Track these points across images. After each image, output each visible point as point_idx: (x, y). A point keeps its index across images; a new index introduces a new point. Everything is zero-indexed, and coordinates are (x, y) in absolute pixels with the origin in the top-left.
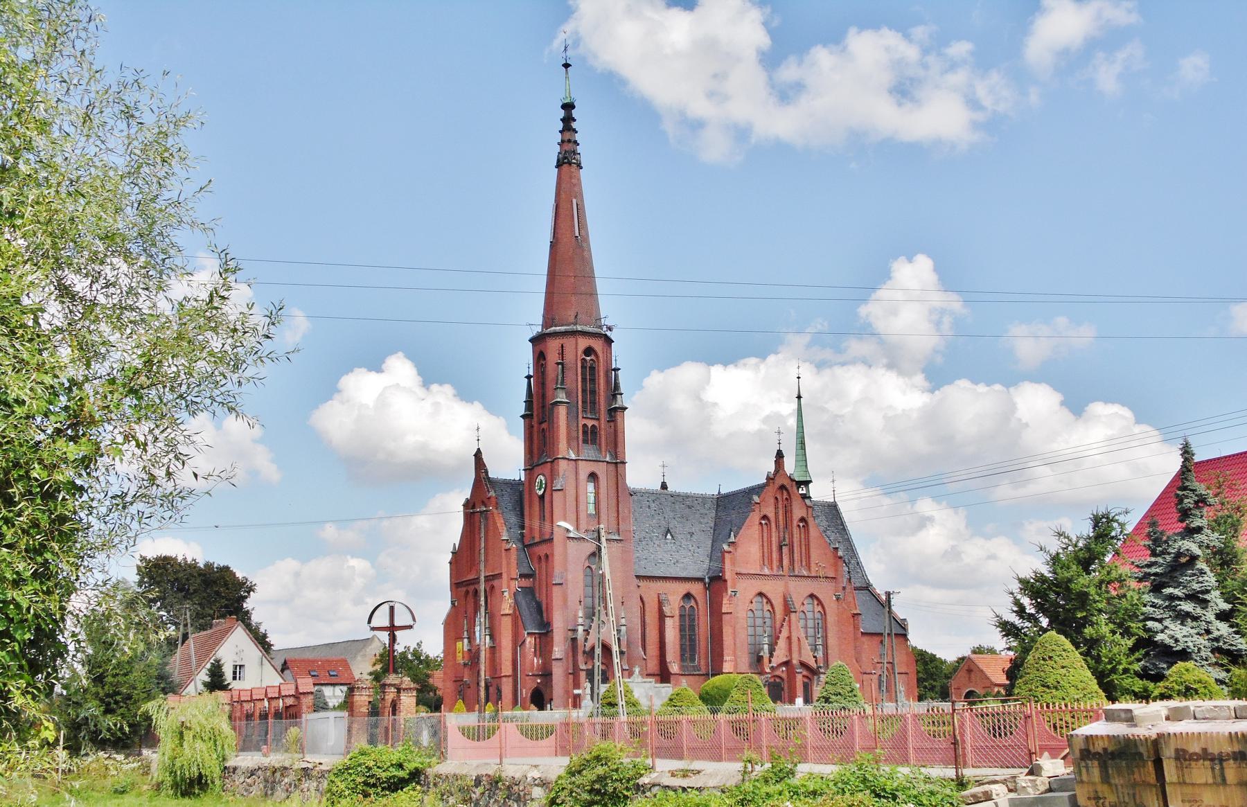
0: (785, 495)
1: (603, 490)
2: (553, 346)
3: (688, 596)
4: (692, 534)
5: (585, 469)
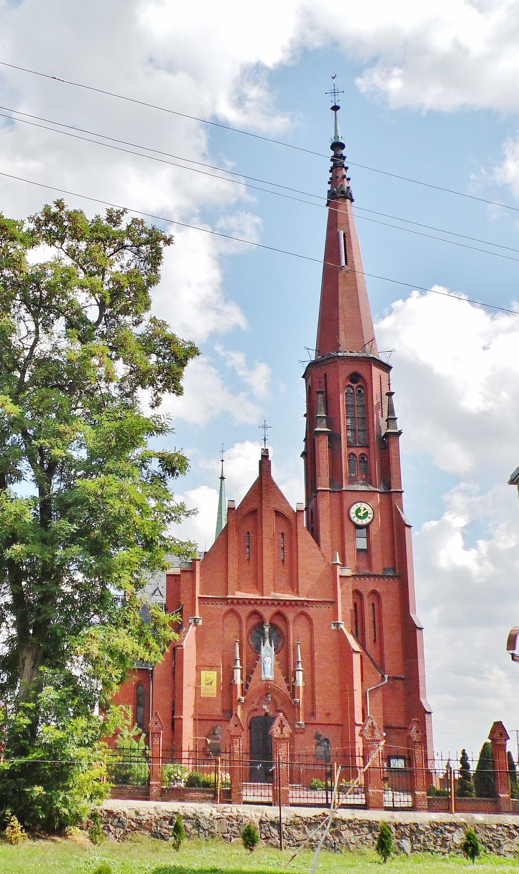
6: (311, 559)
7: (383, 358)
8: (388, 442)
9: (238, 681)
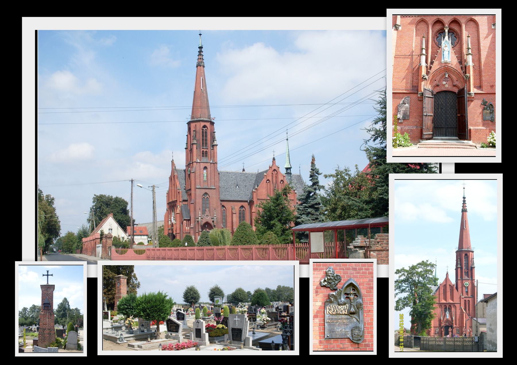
0: (276, 172)
1: (209, 172)
2: (193, 125)
3: (242, 207)
4: (246, 186)
5: (202, 165)
6: (456, 294)
7: (472, 250)
8: (472, 268)
9: (423, 64)
